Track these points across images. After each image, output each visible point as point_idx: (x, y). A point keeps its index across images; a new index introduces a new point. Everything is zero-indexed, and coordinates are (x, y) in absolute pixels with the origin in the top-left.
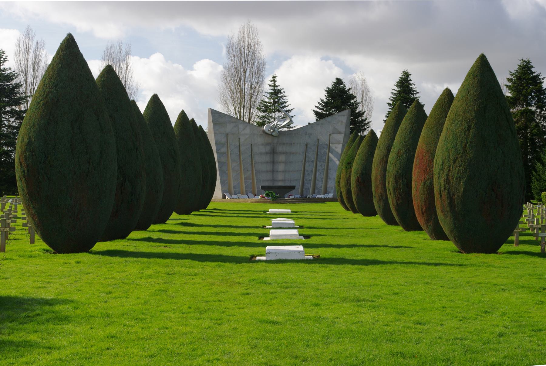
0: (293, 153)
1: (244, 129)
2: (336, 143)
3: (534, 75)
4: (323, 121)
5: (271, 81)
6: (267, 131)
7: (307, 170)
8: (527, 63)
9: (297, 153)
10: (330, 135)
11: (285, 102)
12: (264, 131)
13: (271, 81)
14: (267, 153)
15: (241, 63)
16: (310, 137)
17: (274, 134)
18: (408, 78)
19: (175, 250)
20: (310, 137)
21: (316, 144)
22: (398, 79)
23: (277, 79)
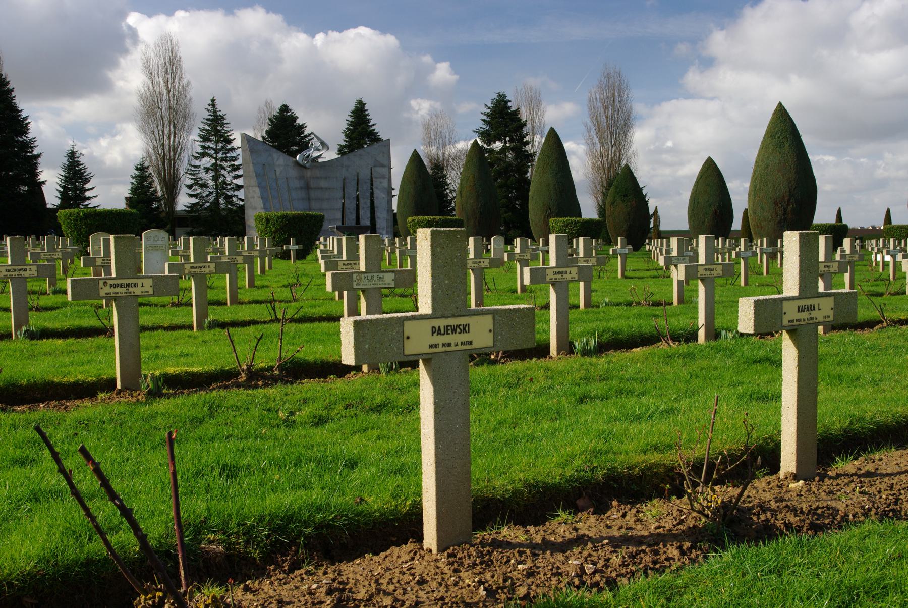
0: (329, 189)
1: (278, 159)
2: (380, 178)
3: (81, 167)
4: (345, 157)
5: (209, 105)
6: (301, 162)
7: (349, 209)
8: (267, 383)
9: (334, 188)
10: (371, 168)
11: (484, 120)
12: (297, 163)
13: (209, 105)
14: (301, 188)
15: (530, 114)
16: (347, 170)
17: (307, 165)
18: (364, 108)
19: (169, 318)
20: (347, 170)
21: (356, 178)
22: (353, 108)
23: (217, 102)
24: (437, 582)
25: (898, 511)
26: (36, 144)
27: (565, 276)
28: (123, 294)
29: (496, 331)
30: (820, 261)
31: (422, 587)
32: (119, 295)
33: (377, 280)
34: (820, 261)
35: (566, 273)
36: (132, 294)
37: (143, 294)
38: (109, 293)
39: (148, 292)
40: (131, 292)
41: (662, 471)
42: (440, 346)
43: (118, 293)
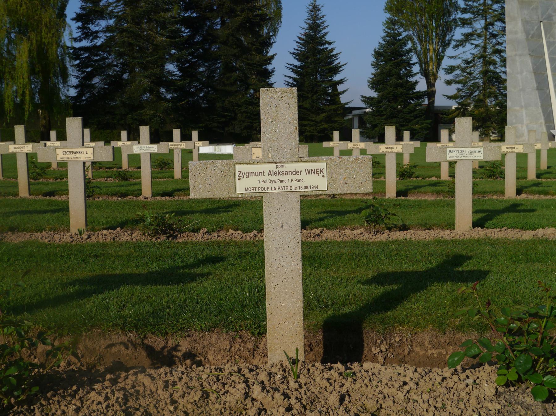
24: (133, 253)
25: (31, 178)
26: (369, 79)
27: (393, 150)
28: (73, 159)
29: (233, 177)
30: (409, 132)
31: (358, 412)
32: (70, 159)
33: (468, 154)
34: (409, 132)
35: (393, 148)
36: (79, 159)
37: (87, 159)
38: (63, 158)
39: (90, 158)
40: (78, 158)
41: (179, 235)
42: (257, 189)
43: (69, 158)
